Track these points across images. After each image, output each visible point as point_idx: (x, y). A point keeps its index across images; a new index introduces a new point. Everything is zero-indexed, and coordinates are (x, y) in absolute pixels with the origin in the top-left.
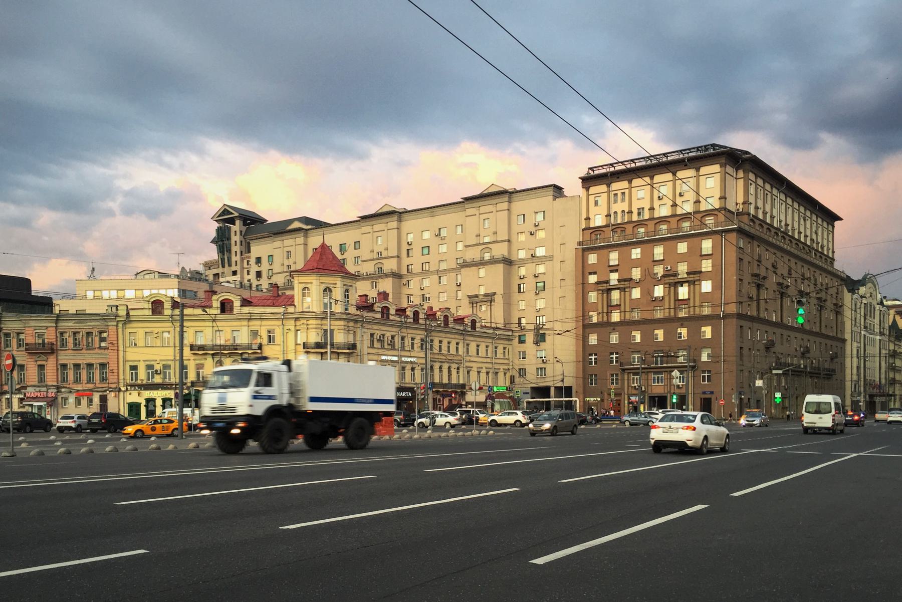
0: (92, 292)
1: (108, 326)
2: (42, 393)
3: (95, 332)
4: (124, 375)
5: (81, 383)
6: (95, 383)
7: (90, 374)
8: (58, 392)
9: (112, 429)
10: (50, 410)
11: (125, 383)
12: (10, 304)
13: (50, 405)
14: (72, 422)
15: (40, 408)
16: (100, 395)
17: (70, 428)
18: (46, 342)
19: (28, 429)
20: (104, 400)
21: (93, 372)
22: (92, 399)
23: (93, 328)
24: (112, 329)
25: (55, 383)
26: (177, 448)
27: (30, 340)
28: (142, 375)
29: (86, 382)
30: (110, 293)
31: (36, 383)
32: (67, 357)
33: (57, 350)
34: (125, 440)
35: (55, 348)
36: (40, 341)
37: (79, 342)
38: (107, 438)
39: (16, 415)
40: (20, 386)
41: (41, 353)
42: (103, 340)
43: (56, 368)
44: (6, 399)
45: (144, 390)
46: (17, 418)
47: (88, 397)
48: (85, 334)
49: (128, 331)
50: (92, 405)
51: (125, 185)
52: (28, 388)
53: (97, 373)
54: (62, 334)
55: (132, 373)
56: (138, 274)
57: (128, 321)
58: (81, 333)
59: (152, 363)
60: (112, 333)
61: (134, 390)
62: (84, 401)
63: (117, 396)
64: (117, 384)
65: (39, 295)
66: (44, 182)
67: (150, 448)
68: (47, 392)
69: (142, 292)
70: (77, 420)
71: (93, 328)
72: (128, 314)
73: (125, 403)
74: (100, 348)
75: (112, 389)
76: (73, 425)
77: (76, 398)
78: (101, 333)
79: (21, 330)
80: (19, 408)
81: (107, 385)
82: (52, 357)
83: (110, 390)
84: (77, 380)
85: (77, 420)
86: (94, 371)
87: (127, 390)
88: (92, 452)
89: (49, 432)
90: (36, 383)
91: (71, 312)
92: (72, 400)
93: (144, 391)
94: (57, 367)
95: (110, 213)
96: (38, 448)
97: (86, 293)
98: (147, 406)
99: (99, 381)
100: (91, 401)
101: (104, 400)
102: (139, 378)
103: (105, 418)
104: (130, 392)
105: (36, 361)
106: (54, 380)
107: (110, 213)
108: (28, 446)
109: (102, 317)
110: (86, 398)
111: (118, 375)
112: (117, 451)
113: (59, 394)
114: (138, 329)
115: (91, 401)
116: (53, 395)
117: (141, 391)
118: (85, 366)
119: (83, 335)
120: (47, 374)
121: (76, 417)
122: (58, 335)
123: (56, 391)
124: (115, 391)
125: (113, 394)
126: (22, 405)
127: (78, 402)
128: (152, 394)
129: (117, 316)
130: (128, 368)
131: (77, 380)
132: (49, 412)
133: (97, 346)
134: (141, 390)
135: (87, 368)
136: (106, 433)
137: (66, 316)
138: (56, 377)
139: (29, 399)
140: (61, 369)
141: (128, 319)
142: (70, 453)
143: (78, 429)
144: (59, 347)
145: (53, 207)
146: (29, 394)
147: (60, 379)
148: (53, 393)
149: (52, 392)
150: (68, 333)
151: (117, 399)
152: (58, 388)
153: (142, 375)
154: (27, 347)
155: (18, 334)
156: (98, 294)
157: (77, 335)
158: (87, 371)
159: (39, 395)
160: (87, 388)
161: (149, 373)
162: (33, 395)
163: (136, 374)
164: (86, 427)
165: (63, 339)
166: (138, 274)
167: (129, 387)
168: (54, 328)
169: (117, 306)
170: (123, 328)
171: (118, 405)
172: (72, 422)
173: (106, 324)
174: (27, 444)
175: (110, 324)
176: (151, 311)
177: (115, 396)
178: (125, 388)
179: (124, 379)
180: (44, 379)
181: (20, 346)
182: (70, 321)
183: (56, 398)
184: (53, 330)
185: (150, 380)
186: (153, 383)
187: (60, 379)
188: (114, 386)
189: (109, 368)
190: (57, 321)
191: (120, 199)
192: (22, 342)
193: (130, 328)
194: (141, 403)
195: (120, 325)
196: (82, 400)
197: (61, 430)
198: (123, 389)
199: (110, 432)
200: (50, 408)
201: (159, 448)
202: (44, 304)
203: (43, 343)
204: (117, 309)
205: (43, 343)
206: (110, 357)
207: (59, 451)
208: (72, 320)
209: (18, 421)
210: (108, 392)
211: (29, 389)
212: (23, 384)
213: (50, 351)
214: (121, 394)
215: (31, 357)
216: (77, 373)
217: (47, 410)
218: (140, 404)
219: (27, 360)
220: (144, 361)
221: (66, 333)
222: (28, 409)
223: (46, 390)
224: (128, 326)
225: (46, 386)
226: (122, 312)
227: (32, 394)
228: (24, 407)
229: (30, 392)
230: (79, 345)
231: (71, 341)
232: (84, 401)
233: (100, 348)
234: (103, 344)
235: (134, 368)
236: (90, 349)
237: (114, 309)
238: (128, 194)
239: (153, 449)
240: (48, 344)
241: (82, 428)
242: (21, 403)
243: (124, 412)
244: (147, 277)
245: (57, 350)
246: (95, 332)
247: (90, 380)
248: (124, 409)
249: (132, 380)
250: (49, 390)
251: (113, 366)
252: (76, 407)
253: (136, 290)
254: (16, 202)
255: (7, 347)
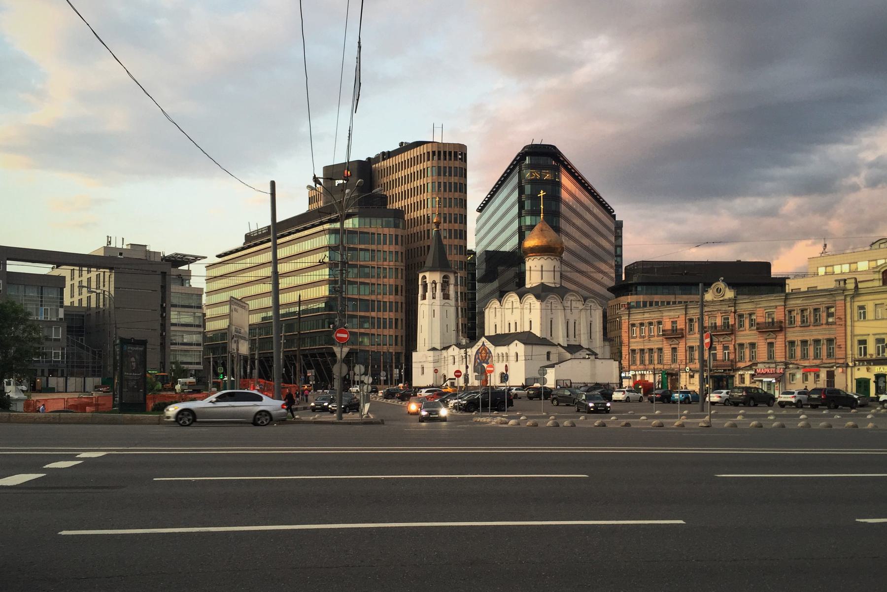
0: (848, 265)
1: (835, 301)
2: (771, 369)
3: (822, 308)
4: (852, 351)
5: (808, 360)
6: (822, 359)
7: (817, 350)
8: (786, 368)
9: (832, 405)
10: (778, 385)
11: (853, 359)
12: (756, 287)
13: (778, 381)
14: (793, 397)
15: (769, 383)
16: (827, 371)
17: (790, 403)
18: (775, 320)
19: (752, 403)
20: (831, 376)
21: (820, 348)
22: (819, 375)
23: (820, 304)
24: (840, 304)
25: (783, 360)
26: (877, 427)
27: (761, 320)
28: (871, 349)
29: (813, 358)
30: (841, 268)
31: (766, 360)
32: (795, 335)
33: (785, 328)
34: (839, 417)
35: (784, 326)
36: (770, 320)
37: (807, 319)
38: (825, 414)
39: (742, 389)
40: (751, 363)
41: (726, 334)
42: (830, 315)
43: (784, 345)
44: (739, 375)
45: (874, 365)
46: (742, 392)
47: (815, 374)
48: (812, 311)
49: (857, 304)
50: (819, 381)
51: (870, 156)
52: (759, 365)
53: (656, 356)
54: (790, 312)
55: (861, 348)
56: (873, 244)
57: (857, 294)
58: (809, 310)
59: (883, 336)
60: (840, 308)
61: (863, 365)
62: (811, 377)
63: (845, 371)
64: (844, 360)
65: (778, 276)
66: (790, 171)
67: (846, 425)
68: (776, 368)
69: (833, 269)
70: (797, 395)
71: (820, 304)
72: (856, 287)
73: (853, 379)
74: (828, 323)
75: (839, 365)
76: (793, 400)
77: (803, 373)
78: (828, 308)
79: (753, 310)
80: (750, 384)
81: (834, 361)
82: (781, 334)
83: (837, 365)
84: (805, 356)
85: (797, 395)
86: (821, 347)
87: (855, 365)
88: (783, 426)
89: (772, 406)
90: (766, 360)
91: (802, 290)
92: (799, 376)
93: (874, 367)
94: (785, 344)
95: (855, 188)
96: (755, 420)
97: (818, 270)
98: (876, 382)
99: (826, 357)
100: (817, 376)
101: (831, 376)
102: (868, 353)
103: (824, 394)
104: (858, 367)
105: (766, 339)
106: (782, 356)
107: (855, 188)
108: (743, 418)
109: (830, 293)
110: (813, 374)
111: (846, 351)
112: (810, 427)
113: (787, 370)
114: (868, 302)
115: (818, 376)
116: (782, 371)
117: (870, 367)
118: (812, 343)
119: (810, 312)
120: (776, 351)
121: (796, 393)
122: (787, 313)
123: (784, 367)
124: (842, 367)
125: (840, 370)
126: (753, 381)
127: (805, 378)
128: (882, 369)
129: (844, 290)
130: (856, 343)
131: (805, 356)
132: (777, 387)
133: (824, 322)
134: (870, 365)
135: (750, 348)
136: (825, 409)
137: (794, 295)
138: (784, 354)
139: (759, 375)
140: (789, 346)
141: (857, 292)
142: (762, 427)
143: (799, 405)
144: (787, 324)
145: (796, 193)
146: (760, 370)
147: (788, 356)
148: (782, 369)
149: (780, 369)
150: (796, 312)
151: (845, 374)
152: (786, 364)
153: (871, 349)
154: (664, 333)
155: (750, 315)
156: (829, 269)
157: (804, 312)
158: (814, 348)
159: (768, 371)
160: (814, 364)
161: (879, 347)
162: (763, 371)
163: (865, 348)
164: (806, 402)
165: (791, 317)
166: (873, 244)
167: (857, 363)
168: (783, 307)
169: (845, 280)
170: (851, 301)
171: (845, 382)
172: (793, 397)
173: (834, 299)
174: (743, 417)
175: (837, 298)
176: (881, 282)
177: (843, 372)
178: (853, 363)
179: (852, 354)
180: (795, 356)
181: (752, 326)
182: (798, 299)
183: (784, 374)
184: (781, 309)
185: (881, 355)
186: (883, 357)
187: (788, 356)
188: (841, 361)
189: (836, 343)
190: (786, 300)
191: (864, 173)
192: (753, 322)
193: (859, 302)
194: (870, 379)
195: (848, 299)
196: (809, 376)
197: (783, 405)
198: (850, 364)
199: (829, 408)
200: (778, 383)
201: (856, 426)
202: (779, 284)
203: (773, 322)
204: (845, 283)
205: (773, 322)
206: (838, 332)
207: (774, 425)
208: (800, 297)
209: (742, 395)
210: (835, 367)
211: (760, 366)
212: (754, 361)
213: (779, 329)
214: (849, 370)
215: (761, 335)
216: (804, 349)
217: (776, 386)
218: (869, 380)
219: (758, 338)
220: (873, 334)
221: (794, 310)
222: (758, 385)
223: (775, 367)
224: (857, 299)
225: (775, 363)
226: (851, 285)
227: (762, 370)
228: (755, 382)
229: (761, 368)
230: (807, 322)
231: (798, 318)
232: (811, 377)
233: (828, 323)
234: (830, 320)
235: (863, 342)
236: (817, 325)
237: (842, 283)
238: (872, 165)
239: (849, 426)
240: (777, 322)
241: (803, 403)
242: (753, 379)
243: (851, 389)
244: (882, 246)
245: (785, 328)
246: (822, 308)
247: (805, 357)
248: (852, 385)
249: (861, 355)
250: (778, 367)
251: (840, 341)
252: (803, 382)
253: (869, 261)
254: (765, 194)
255: (741, 327)
